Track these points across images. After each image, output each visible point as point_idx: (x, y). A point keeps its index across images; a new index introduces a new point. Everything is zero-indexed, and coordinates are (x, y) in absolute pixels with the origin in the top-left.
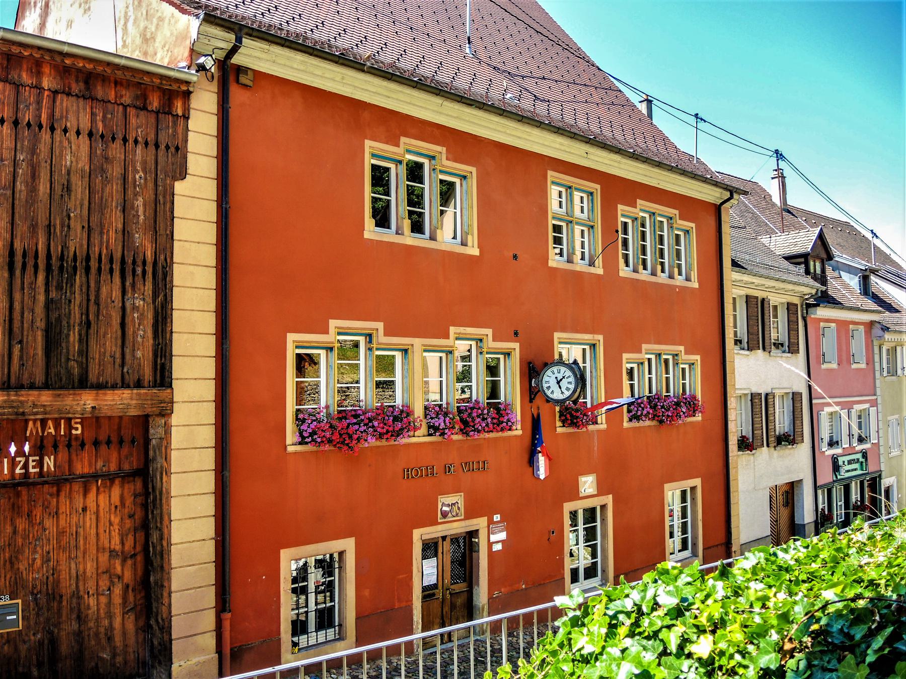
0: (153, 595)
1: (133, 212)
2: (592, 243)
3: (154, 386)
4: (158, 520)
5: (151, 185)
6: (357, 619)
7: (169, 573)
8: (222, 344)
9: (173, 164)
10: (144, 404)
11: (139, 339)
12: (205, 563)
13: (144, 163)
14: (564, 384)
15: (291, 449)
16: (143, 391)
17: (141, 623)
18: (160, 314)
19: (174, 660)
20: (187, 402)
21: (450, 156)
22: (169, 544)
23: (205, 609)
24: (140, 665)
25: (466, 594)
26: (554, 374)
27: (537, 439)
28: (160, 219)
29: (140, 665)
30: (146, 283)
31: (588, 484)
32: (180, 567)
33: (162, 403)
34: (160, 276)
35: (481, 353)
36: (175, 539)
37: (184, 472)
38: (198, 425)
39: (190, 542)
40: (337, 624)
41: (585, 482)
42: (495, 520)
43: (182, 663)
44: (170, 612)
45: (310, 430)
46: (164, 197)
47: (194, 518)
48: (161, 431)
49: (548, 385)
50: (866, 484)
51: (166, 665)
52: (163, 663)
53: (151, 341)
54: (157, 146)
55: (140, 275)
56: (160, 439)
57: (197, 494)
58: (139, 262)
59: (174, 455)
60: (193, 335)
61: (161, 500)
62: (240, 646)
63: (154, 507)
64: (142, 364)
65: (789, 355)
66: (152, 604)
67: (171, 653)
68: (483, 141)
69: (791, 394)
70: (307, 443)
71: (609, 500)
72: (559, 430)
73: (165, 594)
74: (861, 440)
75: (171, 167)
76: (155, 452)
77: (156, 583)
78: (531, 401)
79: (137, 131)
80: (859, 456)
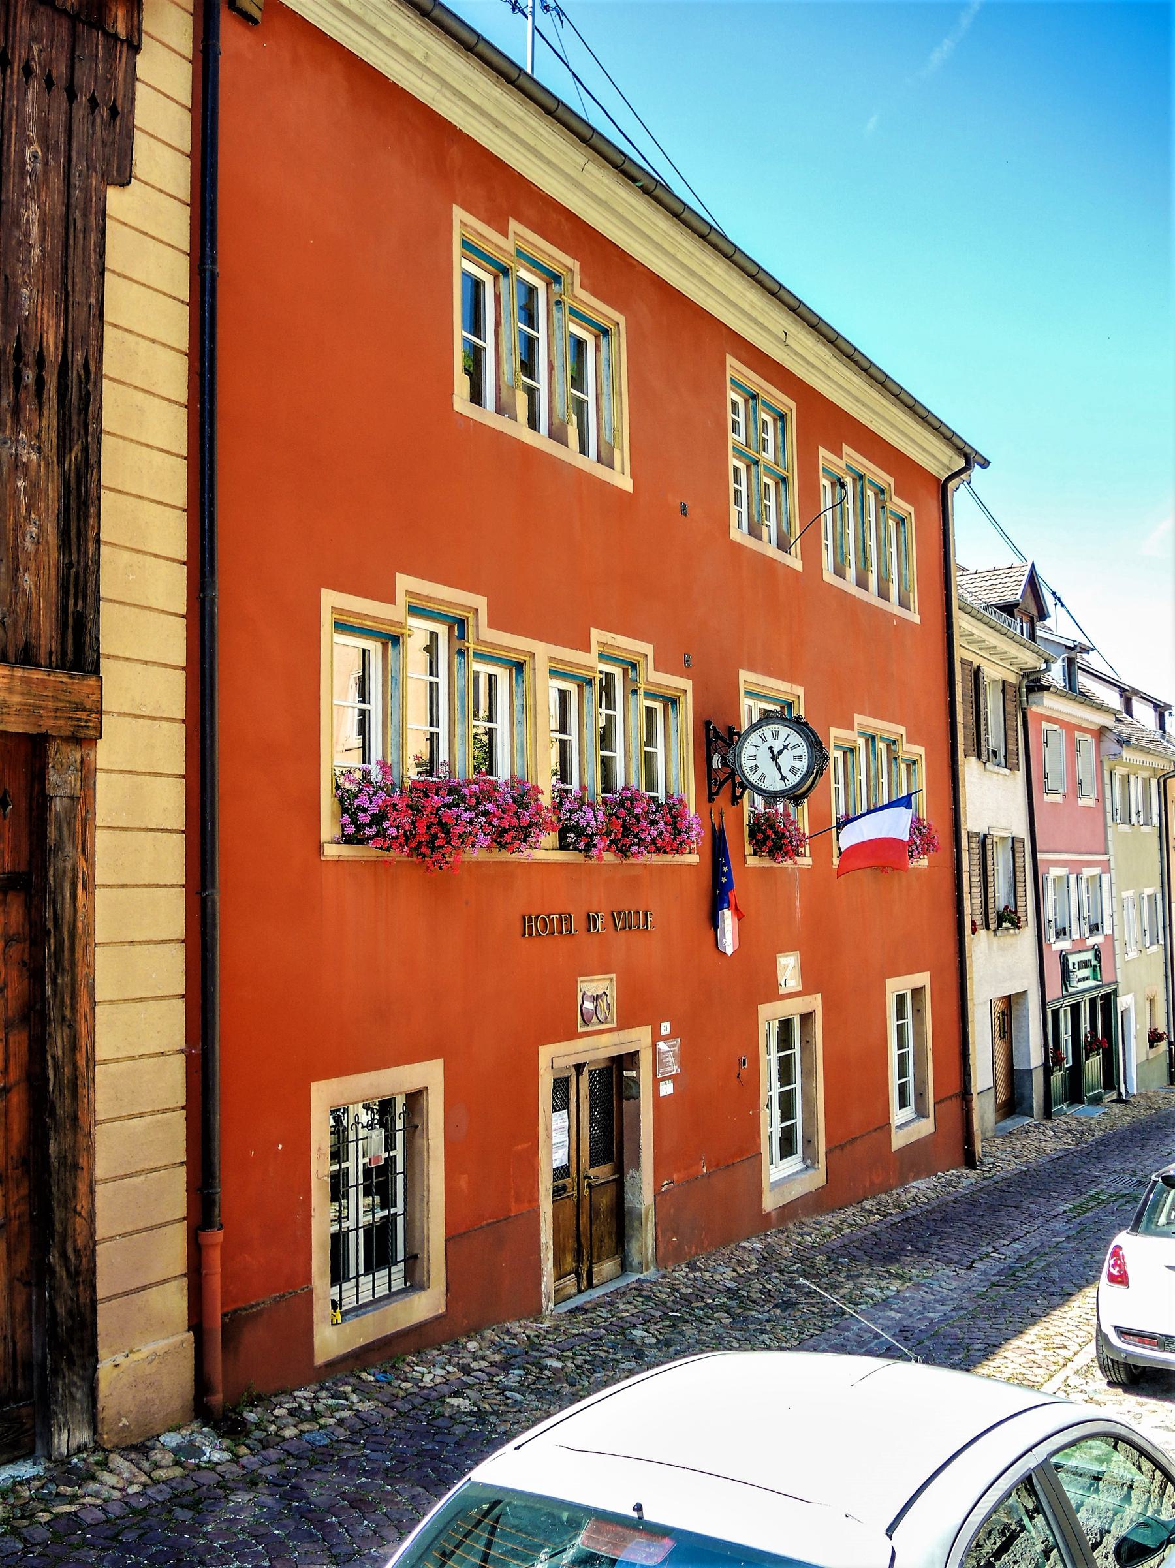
0: (54, 1190)
1: (18, 234)
2: (783, 508)
3: (62, 667)
4: (68, 1001)
5: (56, 181)
6: (447, 1241)
7: (89, 1135)
8: (203, 589)
9: (104, 145)
10: (39, 707)
11: (28, 545)
12: (165, 1111)
13: (44, 125)
14: (786, 760)
15: (332, 851)
16: (37, 675)
17: (21, 1263)
18: (74, 492)
19: (102, 1352)
20: (129, 715)
21: (586, 282)
22: (91, 1062)
23: (166, 1224)
24: (20, 1370)
25: (613, 1186)
26: (765, 740)
27: (724, 874)
28: (76, 263)
29: (20, 1370)
30: (45, 412)
31: (789, 969)
32: (115, 1120)
33: (76, 709)
34: (75, 401)
35: (634, 692)
36: (103, 1050)
37: (123, 886)
38: (150, 774)
39: (133, 1058)
40: (401, 1256)
41: (785, 967)
42: (663, 1033)
43: (120, 1359)
44: (93, 1233)
45: (374, 809)
46: (85, 216)
47: (142, 1000)
48: (73, 779)
49: (753, 763)
50: (1099, 1002)
51: (84, 1367)
52: (79, 1362)
53: (54, 555)
54: (72, 94)
55: (32, 388)
56: (72, 798)
57: (148, 942)
58: (30, 357)
59: (102, 841)
60: (141, 556)
61: (72, 950)
62: (235, 1311)
63: (57, 969)
64: (35, 608)
65: (1007, 771)
66: (51, 1209)
67: (94, 1335)
68: (631, 265)
69: (1010, 840)
70: (361, 842)
71: (815, 1003)
72: (752, 861)
73: (82, 1188)
74: (1095, 928)
75: (100, 149)
76: (60, 830)
77: (62, 1159)
78: (711, 799)
79: (30, 48)
80: (1089, 956)
